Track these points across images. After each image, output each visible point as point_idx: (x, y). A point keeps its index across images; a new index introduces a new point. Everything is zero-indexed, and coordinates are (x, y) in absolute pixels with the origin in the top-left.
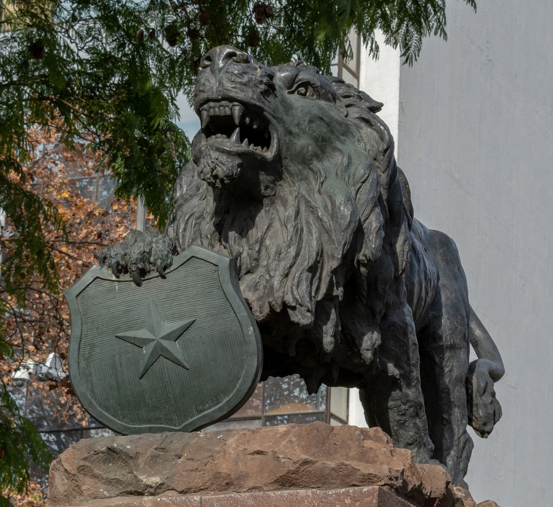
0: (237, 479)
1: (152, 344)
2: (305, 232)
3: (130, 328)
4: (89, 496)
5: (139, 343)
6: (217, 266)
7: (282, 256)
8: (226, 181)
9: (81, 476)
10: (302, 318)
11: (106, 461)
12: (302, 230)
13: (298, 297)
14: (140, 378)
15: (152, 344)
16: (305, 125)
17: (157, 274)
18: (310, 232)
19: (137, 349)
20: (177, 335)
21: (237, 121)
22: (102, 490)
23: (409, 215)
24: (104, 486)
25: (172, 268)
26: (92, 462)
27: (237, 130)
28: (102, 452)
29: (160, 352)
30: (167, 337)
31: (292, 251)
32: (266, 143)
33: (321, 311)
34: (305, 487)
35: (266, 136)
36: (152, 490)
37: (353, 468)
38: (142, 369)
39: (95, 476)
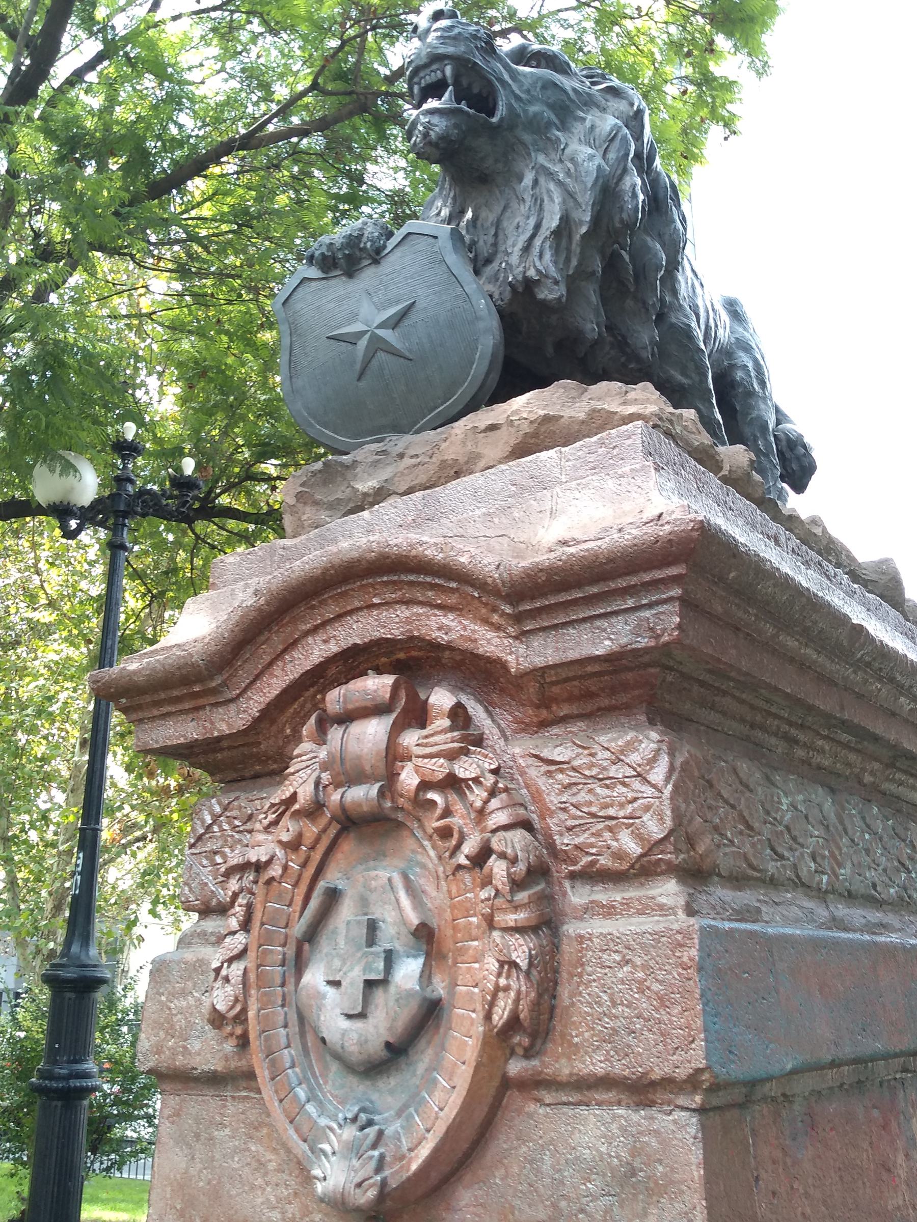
0: (467, 463)
1: (367, 336)
2: (546, 202)
3: (338, 328)
4: (310, 526)
5: (351, 340)
6: (436, 237)
7: (520, 230)
8: (442, 145)
9: (300, 506)
10: (548, 293)
11: (325, 483)
12: (542, 201)
13: (541, 268)
14: (359, 379)
15: (367, 336)
16: (537, 93)
17: (369, 262)
18: (552, 200)
19: (350, 347)
20: (396, 322)
21: (450, 81)
22: (323, 516)
23: (756, 874)
24: (327, 513)
25: (386, 251)
26: (311, 486)
27: (451, 88)
28: (320, 471)
29: (377, 345)
30: (381, 326)
31: (532, 222)
32: (491, 114)
33: (573, 282)
34: (547, 448)
35: (491, 105)
36: (371, 500)
37: (608, 412)
38: (358, 367)
39: (316, 503)
